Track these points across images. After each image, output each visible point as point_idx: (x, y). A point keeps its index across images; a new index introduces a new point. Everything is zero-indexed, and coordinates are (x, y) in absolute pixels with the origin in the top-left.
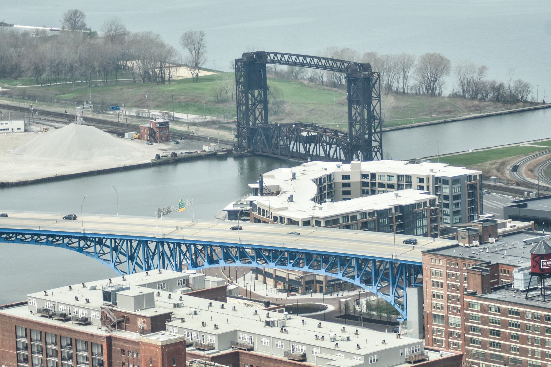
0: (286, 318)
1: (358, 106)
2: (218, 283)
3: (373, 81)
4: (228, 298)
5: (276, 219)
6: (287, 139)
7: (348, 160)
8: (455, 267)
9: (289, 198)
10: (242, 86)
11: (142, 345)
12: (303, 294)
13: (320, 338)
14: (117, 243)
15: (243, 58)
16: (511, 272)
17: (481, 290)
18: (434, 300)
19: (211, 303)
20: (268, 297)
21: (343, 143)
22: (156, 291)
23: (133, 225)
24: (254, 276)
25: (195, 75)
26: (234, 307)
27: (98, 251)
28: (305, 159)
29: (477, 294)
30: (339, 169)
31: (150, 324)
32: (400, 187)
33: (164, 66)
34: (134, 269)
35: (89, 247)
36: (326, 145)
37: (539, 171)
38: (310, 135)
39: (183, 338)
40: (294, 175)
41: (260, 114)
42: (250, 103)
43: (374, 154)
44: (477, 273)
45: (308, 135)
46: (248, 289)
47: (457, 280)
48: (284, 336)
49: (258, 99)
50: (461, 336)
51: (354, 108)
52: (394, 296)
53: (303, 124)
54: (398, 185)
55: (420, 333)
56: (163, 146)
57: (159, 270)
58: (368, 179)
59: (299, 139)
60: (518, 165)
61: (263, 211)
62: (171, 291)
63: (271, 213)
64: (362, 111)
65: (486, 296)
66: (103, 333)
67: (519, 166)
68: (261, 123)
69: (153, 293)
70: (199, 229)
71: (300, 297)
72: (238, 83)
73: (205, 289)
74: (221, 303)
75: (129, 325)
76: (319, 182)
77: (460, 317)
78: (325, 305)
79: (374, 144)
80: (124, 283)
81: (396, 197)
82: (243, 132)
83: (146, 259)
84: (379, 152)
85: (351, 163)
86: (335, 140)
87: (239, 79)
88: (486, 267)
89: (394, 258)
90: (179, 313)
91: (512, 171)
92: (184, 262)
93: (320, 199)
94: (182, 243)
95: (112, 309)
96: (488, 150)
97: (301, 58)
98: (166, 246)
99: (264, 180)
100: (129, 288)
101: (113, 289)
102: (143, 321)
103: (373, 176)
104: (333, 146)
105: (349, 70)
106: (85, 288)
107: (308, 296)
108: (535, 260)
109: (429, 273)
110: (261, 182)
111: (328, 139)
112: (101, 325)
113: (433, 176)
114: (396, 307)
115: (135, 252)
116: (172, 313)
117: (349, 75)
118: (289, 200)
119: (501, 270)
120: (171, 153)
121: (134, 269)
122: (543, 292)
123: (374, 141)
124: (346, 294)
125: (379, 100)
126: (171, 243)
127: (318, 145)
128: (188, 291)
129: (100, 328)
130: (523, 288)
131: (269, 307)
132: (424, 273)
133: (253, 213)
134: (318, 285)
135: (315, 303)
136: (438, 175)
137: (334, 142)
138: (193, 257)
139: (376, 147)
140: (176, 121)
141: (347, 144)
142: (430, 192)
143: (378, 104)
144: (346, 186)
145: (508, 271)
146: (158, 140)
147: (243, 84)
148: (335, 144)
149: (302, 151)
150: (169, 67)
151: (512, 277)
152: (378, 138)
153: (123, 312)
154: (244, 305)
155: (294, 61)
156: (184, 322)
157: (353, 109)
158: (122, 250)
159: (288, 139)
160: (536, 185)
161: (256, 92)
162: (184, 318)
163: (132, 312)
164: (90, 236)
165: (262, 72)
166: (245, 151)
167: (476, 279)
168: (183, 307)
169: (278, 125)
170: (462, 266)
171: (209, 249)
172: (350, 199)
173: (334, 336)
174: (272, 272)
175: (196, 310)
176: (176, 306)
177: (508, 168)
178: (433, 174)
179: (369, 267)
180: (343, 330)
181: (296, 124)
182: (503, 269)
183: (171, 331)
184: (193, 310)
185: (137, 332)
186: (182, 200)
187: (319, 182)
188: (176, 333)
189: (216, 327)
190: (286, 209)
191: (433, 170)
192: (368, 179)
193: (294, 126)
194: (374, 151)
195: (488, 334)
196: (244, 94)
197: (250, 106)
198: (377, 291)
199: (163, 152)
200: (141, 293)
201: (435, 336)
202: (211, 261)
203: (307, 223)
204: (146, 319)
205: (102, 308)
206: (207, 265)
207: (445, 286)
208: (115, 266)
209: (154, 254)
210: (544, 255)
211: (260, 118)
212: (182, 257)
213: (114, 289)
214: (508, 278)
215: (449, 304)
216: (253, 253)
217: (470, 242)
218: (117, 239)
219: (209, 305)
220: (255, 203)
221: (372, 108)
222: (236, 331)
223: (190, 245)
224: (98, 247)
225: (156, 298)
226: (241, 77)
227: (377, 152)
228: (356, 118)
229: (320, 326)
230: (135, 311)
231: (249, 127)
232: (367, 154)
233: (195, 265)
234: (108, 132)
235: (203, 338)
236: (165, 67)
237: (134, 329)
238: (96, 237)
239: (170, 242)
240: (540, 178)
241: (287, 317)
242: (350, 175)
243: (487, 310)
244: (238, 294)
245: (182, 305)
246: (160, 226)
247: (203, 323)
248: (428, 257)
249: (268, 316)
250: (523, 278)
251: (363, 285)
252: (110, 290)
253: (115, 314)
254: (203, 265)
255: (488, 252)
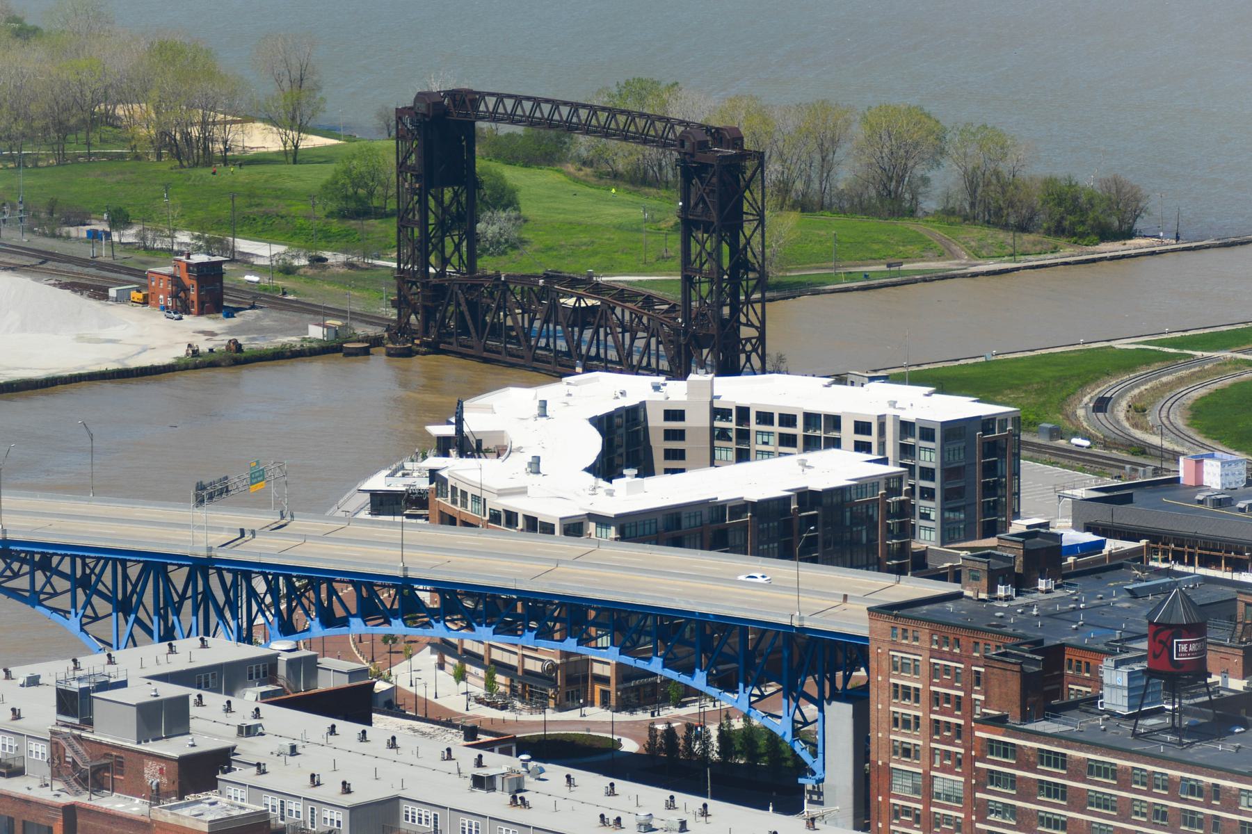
0: (524, 770)
1: (705, 235)
2: (353, 674)
3: (748, 174)
4: (374, 715)
5: (495, 517)
6: (523, 314)
7: (679, 372)
8: (951, 650)
9: (530, 464)
10: (412, 175)
11: (158, 829)
12: (560, 708)
13: (611, 822)
14: (89, 568)
15: (418, 104)
16: (1097, 667)
17: (1018, 711)
18: (896, 733)
19: (333, 727)
20: (469, 713)
21: (666, 329)
22: (193, 693)
23: (44, 514)
24: (435, 657)
25: (290, 143)
26: (394, 738)
27: (38, 588)
28: (202, 309)
29: (1007, 722)
30: (657, 393)
31: (175, 776)
32: (811, 444)
33: (211, 120)
34: (131, 635)
35: (16, 575)
36: (623, 333)
37: (1164, 414)
38: (583, 305)
39: (264, 814)
40: (543, 405)
41: (457, 247)
42: (432, 220)
43: (743, 357)
44: (1010, 667)
45: (577, 305)
46: (421, 693)
47: (956, 684)
48: (518, 815)
49: (453, 209)
50: (963, 827)
51: (697, 241)
52: (794, 721)
53: (564, 278)
54: (807, 438)
55: (856, 816)
56: (206, 323)
57: (202, 639)
58: (731, 421)
59: (553, 314)
60: (1108, 395)
61: (464, 494)
62: (230, 692)
63: (485, 499)
64: (718, 249)
65: (1030, 727)
66: (57, 794)
67: (1111, 398)
68: (458, 272)
69: (185, 699)
70: (300, 536)
71: (551, 715)
72: (402, 169)
73: (316, 691)
74: (361, 727)
75: (122, 778)
76: (603, 424)
77: (962, 779)
78: (616, 738)
79: (745, 332)
80: (110, 669)
81: (801, 468)
82: (412, 294)
83: (162, 611)
84: (758, 354)
85: (689, 378)
86: (645, 320)
87: (405, 158)
88: (1031, 652)
89: (796, 623)
90: (249, 749)
91: (1094, 411)
92: (260, 620)
93: (605, 469)
94: (256, 573)
95: (80, 736)
96: (1033, 357)
97: (565, 111)
98: (214, 581)
99: (466, 415)
100: (123, 684)
101: (84, 685)
102: (158, 768)
103: (743, 413)
104: (640, 334)
105: (687, 144)
106: (10, 681)
107: (573, 715)
108: (1157, 639)
109: (885, 665)
110: (460, 422)
111: (627, 317)
112: (48, 778)
113: (896, 417)
114: (798, 746)
115: (133, 591)
116: (234, 748)
117: (687, 157)
118: (529, 470)
119: (1070, 660)
120: (226, 342)
121: (131, 635)
122: (1177, 721)
123: (744, 325)
124: (669, 712)
125: (761, 221)
126: (229, 570)
127: (602, 330)
128: (274, 693)
129: (47, 785)
130: (1126, 709)
131: (475, 739)
132: (873, 664)
133: (437, 499)
134: (598, 688)
135: (591, 733)
136: (908, 416)
137: (643, 324)
138: (283, 607)
139: (748, 340)
140: (245, 261)
141: (676, 331)
142: (887, 459)
143: (759, 231)
144: (675, 439)
145: (1088, 664)
146: (193, 307)
147: (413, 171)
148: (646, 329)
149: (562, 345)
150: (226, 123)
151: (1099, 683)
152: (755, 318)
153: (106, 745)
154: (412, 733)
155: (527, 114)
156: (264, 772)
157: (693, 243)
158: (100, 587)
159: (526, 315)
160: (1155, 447)
161: (448, 194)
162: (264, 764)
163: (131, 744)
164: (18, 548)
165: (464, 143)
166: (417, 342)
167: (1006, 681)
168: (262, 734)
169: (503, 279)
170: (971, 650)
171: (324, 587)
172: (682, 470)
173: (648, 818)
174: (480, 649)
175: (295, 743)
176: (247, 731)
177: (1086, 399)
178: (897, 412)
179: (729, 645)
180: (671, 804)
181: (547, 276)
182: (1074, 658)
183: (230, 797)
184: (287, 743)
185: (141, 797)
186: (258, 462)
187: (603, 424)
188: (242, 800)
189: (346, 788)
190: (522, 491)
191: (895, 402)
192: (731, 421)
193: (541, 281)
194: (744, 351)
195: (1034, 823)
196: (416, 198)
197: (431, 228)
198: (750, 707)
199: (207, 340)
200: (156, 696)
201: (895, 824)
202: (328, 619)
203: (574, 528)
204: (165, 762)
205: (53, 733)
206: (317, 630)
207: (924, 697)
208: (82, 626)
209: (183, 597)
210: (1183, 625)
211: (455, 260)
212: (255, 608)
213: (87, 685)
214: (1086, 682)
215: (933, 745)
216: (433, 602)
217: (992, 589)
218: (89, 557)
219: (327, 730)
220: (444, 474)
221: (742, 241)
222: (395, 800)
223: (276, 577)
224: (40, 577)
225: (194, 710)
226: (411, 155)
227: (751, 352)
228: (702, 265)
229: (611, 791)
230: (139, 743)
231: (428, 282)
232: (726, 359)
233: (287, 628)
234: (64, 286)
235: (313, 816)
236: (214, 123)
237: (135, 790)
238: (36, 550)
239: (225, 569)
240: (1165, 431)
241: (527, 768)
242: (684, 411)
243: (1034, 762)
244: (392, 705)
245: (260, 730)
246: (200, 527)
247: (313, 776)
248: (884, 625)
249: (479, 763)
250: (1126, 684)
251: (714, 691)
252: (75, 686)
253: (86, 750)
254: (308, 630)
255: (1037, 615)
